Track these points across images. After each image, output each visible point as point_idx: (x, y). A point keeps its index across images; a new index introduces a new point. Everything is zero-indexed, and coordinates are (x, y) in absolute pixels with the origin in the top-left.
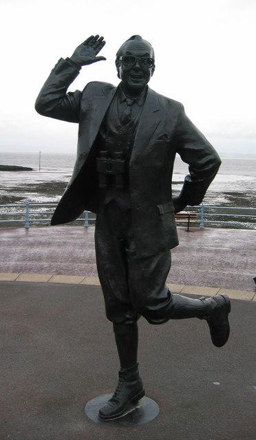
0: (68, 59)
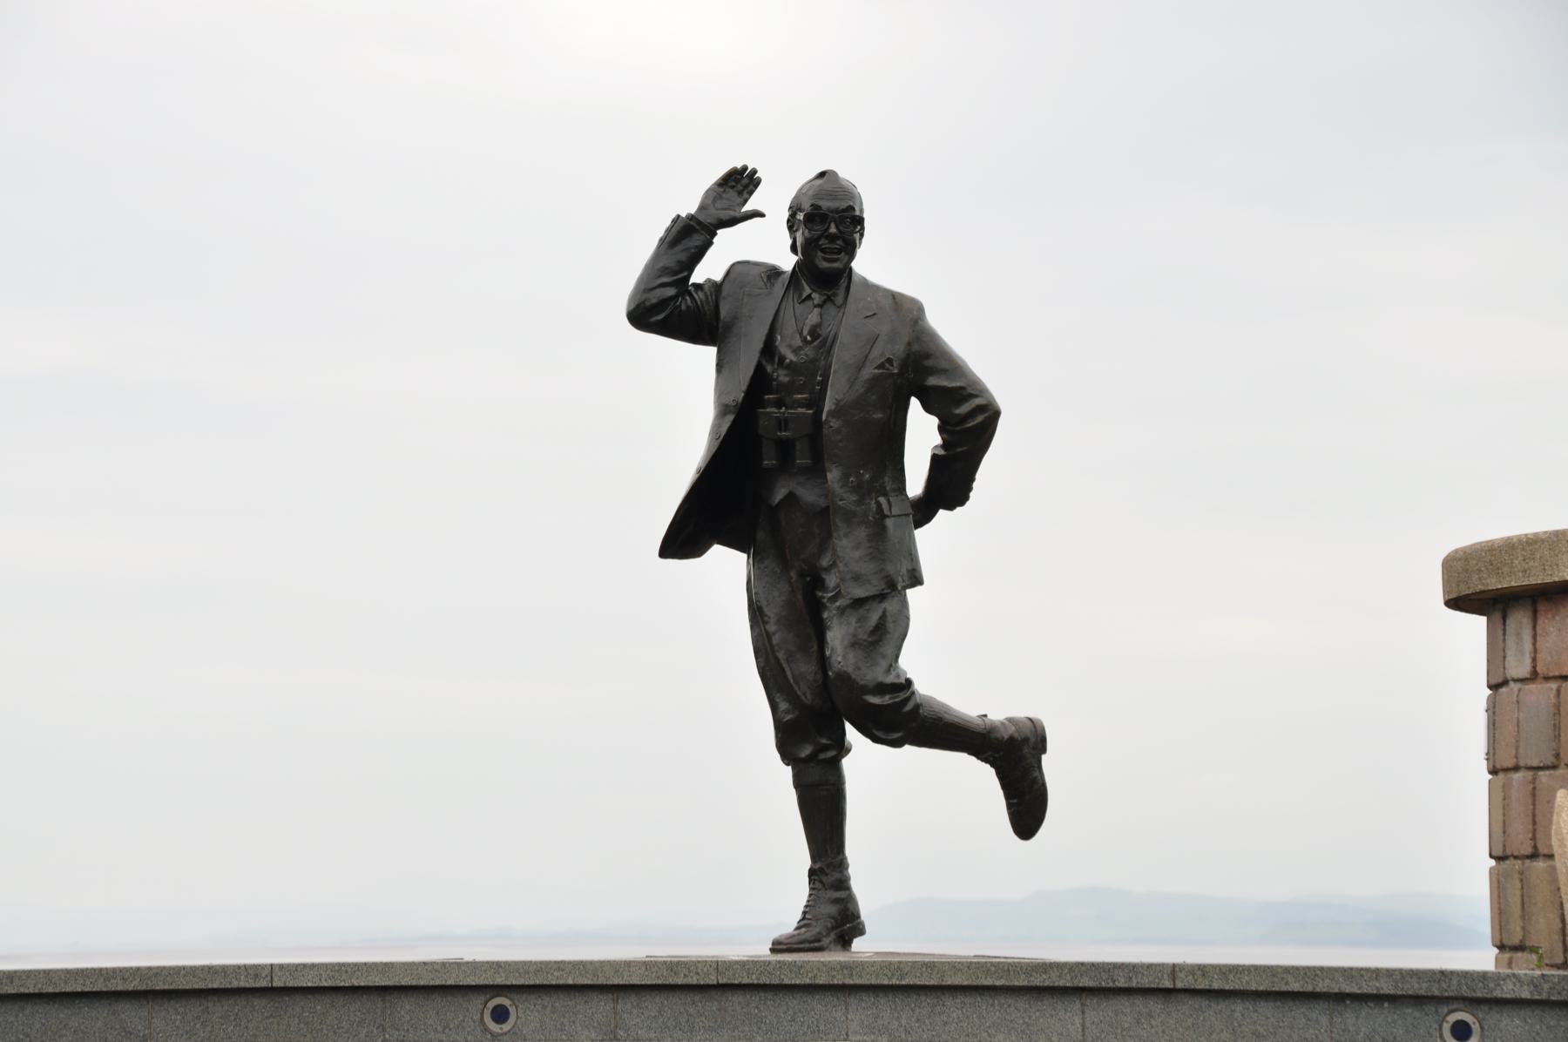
0: (691, 217)
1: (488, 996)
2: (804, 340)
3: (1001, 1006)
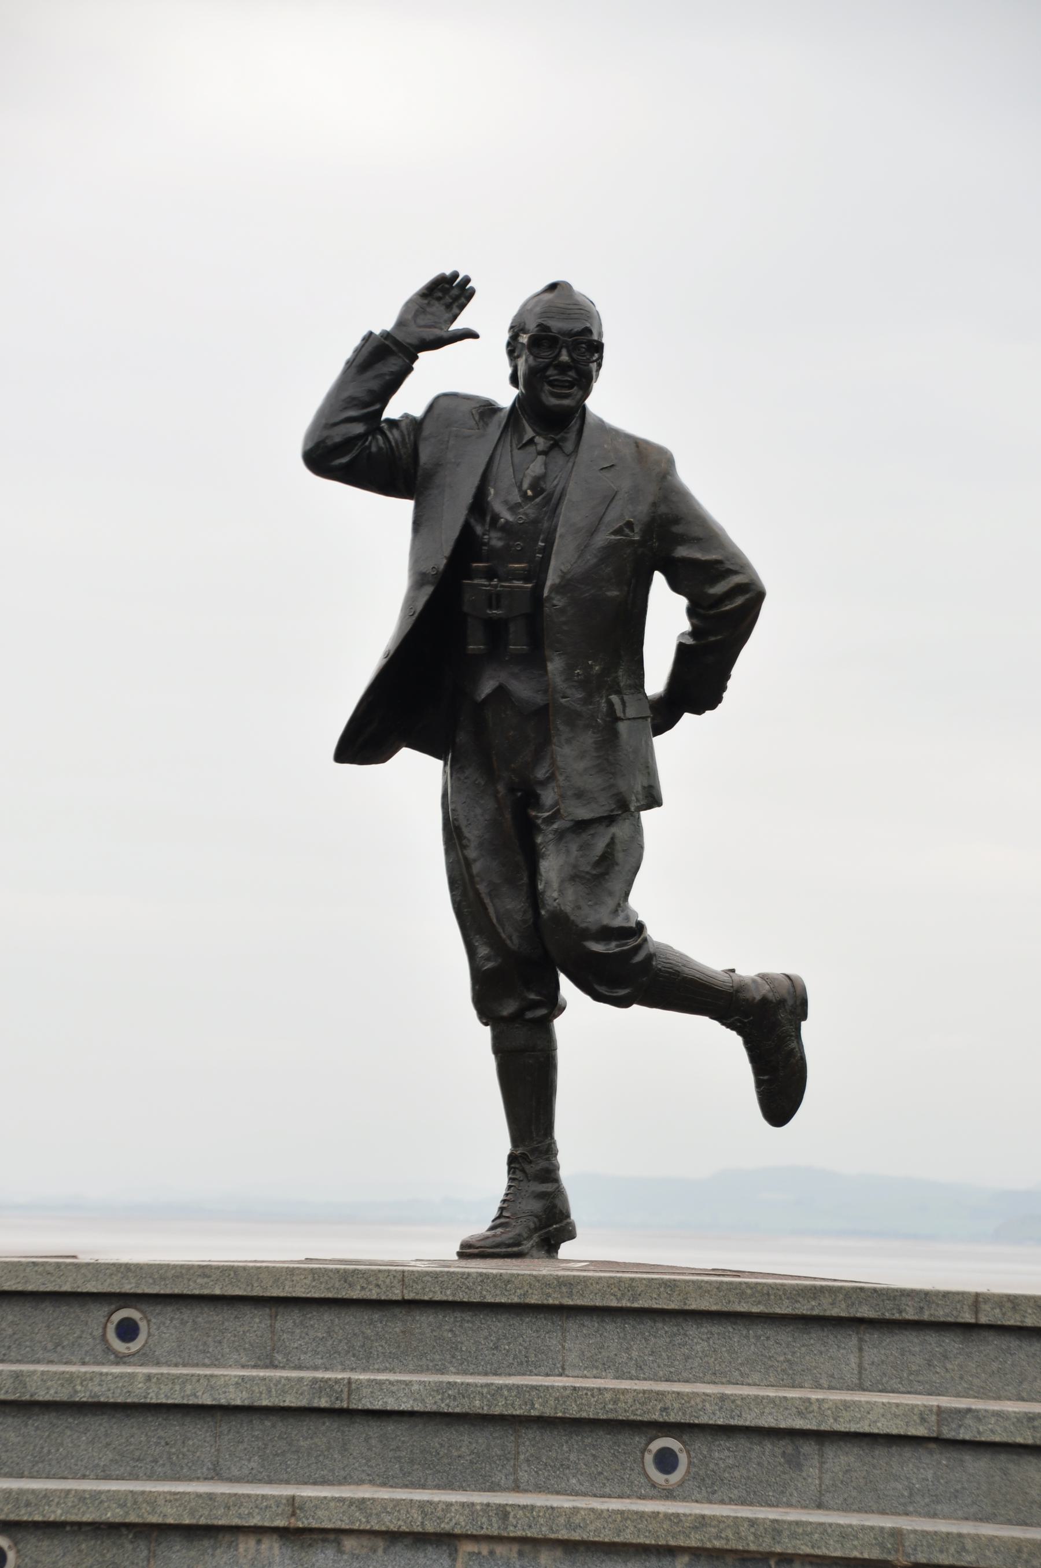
0: (386, 335)
1: (113, 1307)
2: (524, 495)
3: (758, 1338)
